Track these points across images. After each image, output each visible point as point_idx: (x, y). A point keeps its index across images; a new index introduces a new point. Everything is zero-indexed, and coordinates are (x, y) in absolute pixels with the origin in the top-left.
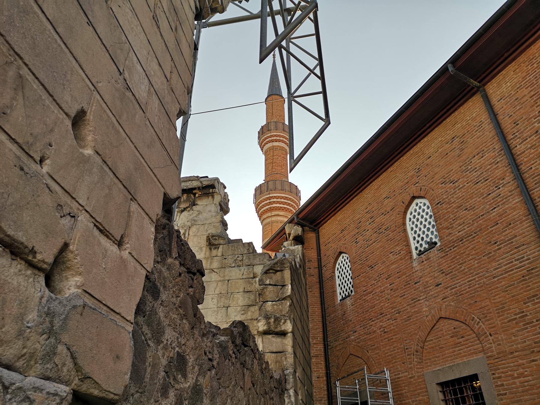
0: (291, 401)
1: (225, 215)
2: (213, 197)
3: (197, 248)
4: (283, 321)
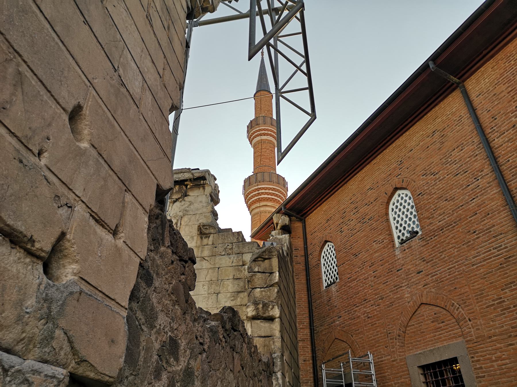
0: (279, 383)
1: (216, 205)
2: (204, 188)
3: (189, 237)
4: (271, 307)
